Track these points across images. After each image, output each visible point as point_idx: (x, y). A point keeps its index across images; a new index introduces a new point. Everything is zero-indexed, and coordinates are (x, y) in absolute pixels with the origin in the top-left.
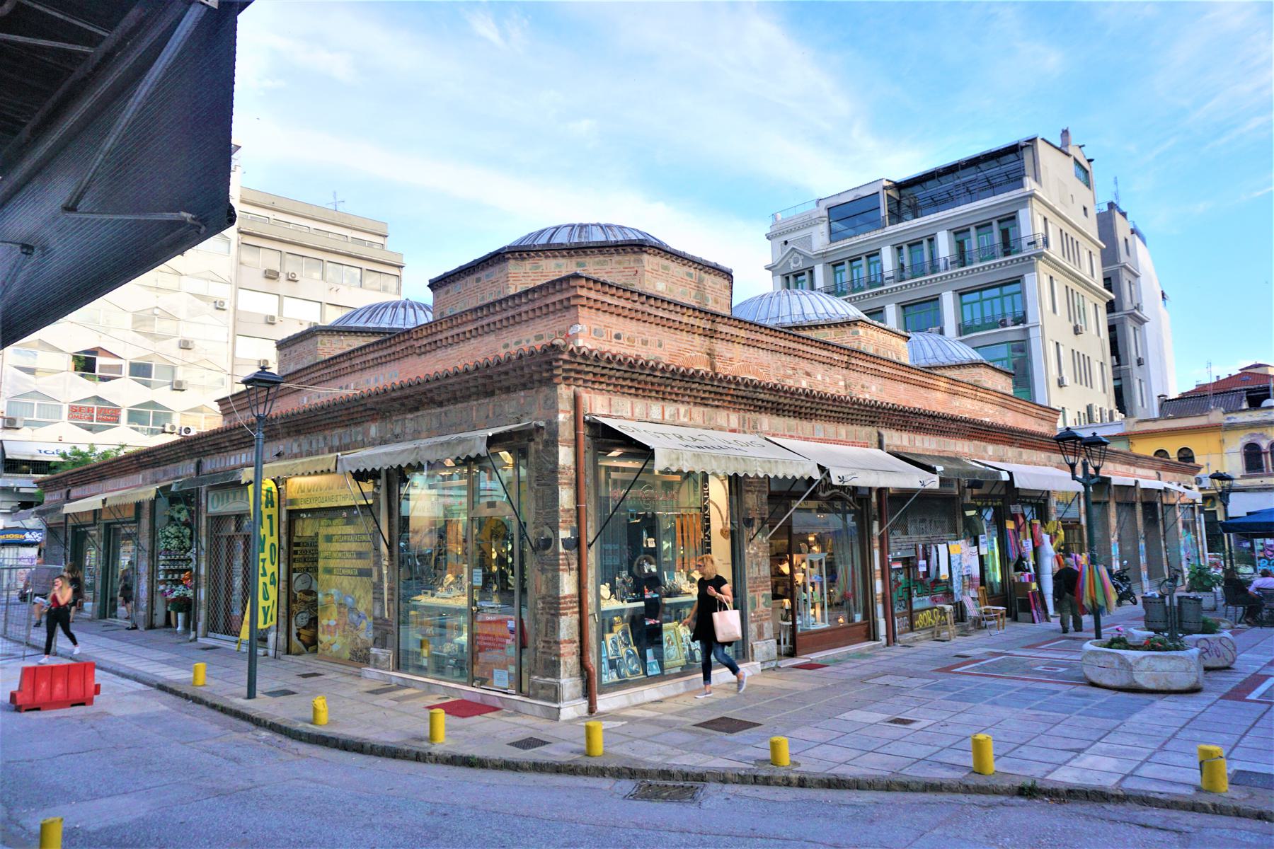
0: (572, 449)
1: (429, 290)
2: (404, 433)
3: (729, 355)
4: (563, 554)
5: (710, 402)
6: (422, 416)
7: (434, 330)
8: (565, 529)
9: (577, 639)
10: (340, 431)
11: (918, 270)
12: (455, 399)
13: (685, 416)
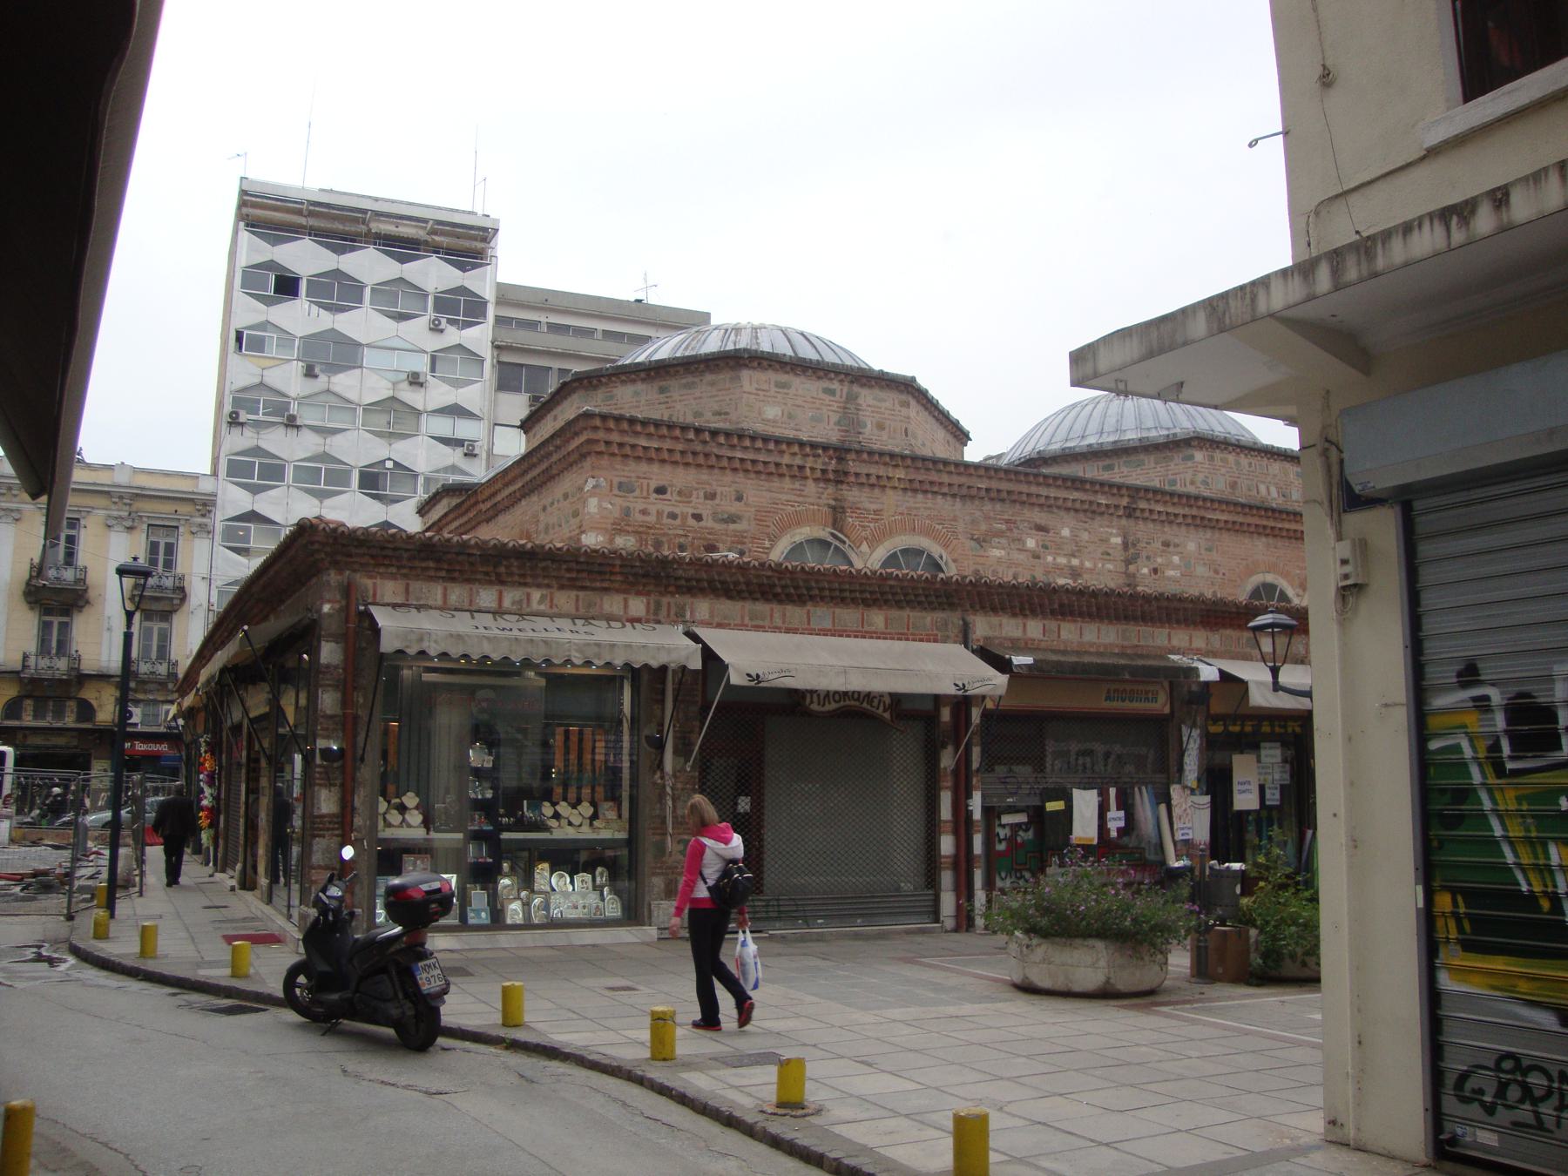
3: (873, 507)
4: (320, 766)
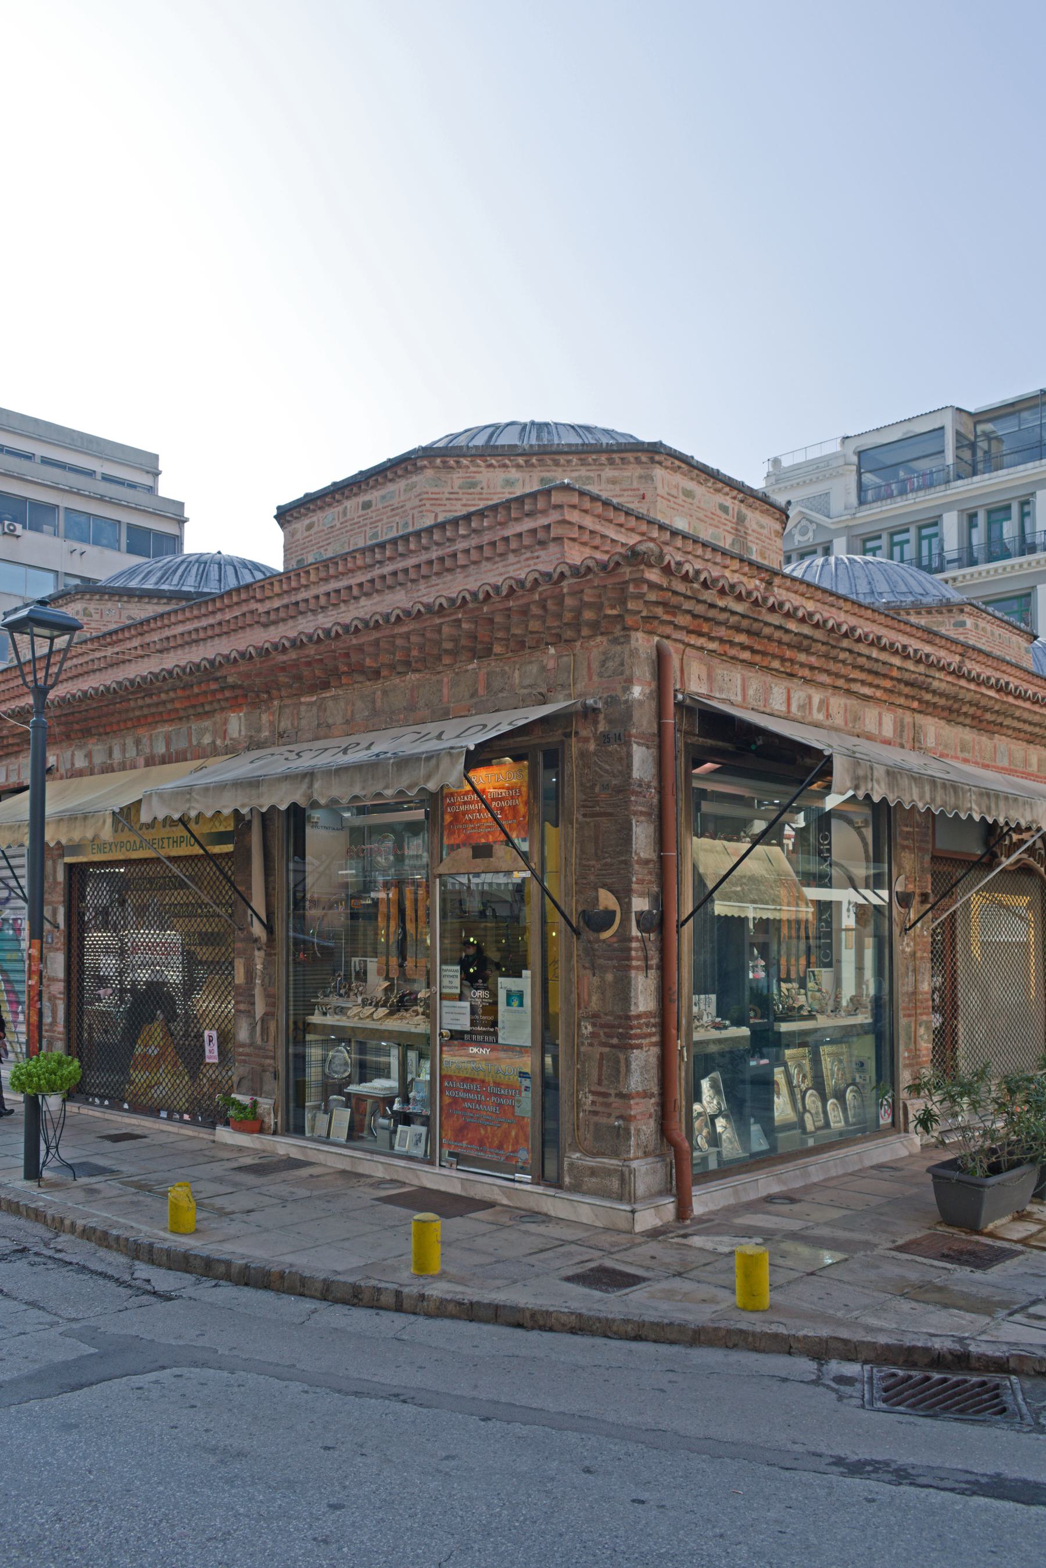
0: (654, 751)
1: (275, 522)
2: (298, 730)
5: (856, 687)
6: (334, 698)
7: (294, 584)
8: (641, 895)
9: (655, 1090)
10: (167, 728)
11: (996, 551)
12: (407, 663)
13: (819, 710)
